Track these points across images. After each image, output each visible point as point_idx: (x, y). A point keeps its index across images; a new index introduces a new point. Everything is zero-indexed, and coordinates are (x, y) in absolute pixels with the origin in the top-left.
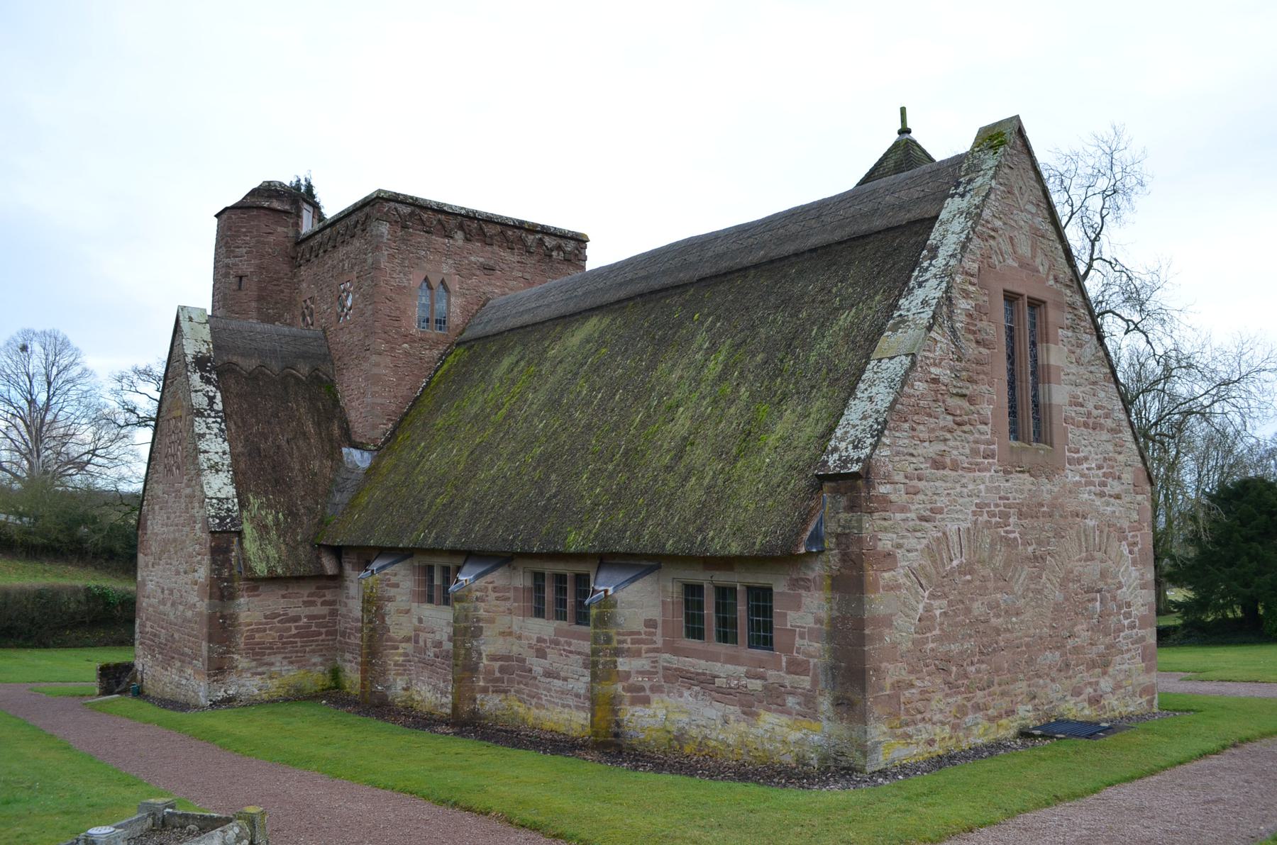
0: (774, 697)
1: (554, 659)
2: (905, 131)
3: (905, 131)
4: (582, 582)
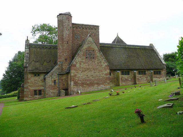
0: (161, 77)
1: (142, 78)
2: (118, 35)
3: (118, 35)
4: (145, 71)
